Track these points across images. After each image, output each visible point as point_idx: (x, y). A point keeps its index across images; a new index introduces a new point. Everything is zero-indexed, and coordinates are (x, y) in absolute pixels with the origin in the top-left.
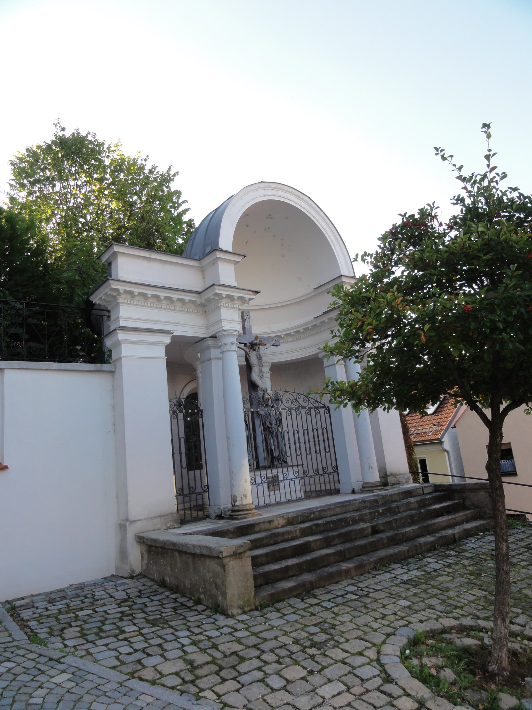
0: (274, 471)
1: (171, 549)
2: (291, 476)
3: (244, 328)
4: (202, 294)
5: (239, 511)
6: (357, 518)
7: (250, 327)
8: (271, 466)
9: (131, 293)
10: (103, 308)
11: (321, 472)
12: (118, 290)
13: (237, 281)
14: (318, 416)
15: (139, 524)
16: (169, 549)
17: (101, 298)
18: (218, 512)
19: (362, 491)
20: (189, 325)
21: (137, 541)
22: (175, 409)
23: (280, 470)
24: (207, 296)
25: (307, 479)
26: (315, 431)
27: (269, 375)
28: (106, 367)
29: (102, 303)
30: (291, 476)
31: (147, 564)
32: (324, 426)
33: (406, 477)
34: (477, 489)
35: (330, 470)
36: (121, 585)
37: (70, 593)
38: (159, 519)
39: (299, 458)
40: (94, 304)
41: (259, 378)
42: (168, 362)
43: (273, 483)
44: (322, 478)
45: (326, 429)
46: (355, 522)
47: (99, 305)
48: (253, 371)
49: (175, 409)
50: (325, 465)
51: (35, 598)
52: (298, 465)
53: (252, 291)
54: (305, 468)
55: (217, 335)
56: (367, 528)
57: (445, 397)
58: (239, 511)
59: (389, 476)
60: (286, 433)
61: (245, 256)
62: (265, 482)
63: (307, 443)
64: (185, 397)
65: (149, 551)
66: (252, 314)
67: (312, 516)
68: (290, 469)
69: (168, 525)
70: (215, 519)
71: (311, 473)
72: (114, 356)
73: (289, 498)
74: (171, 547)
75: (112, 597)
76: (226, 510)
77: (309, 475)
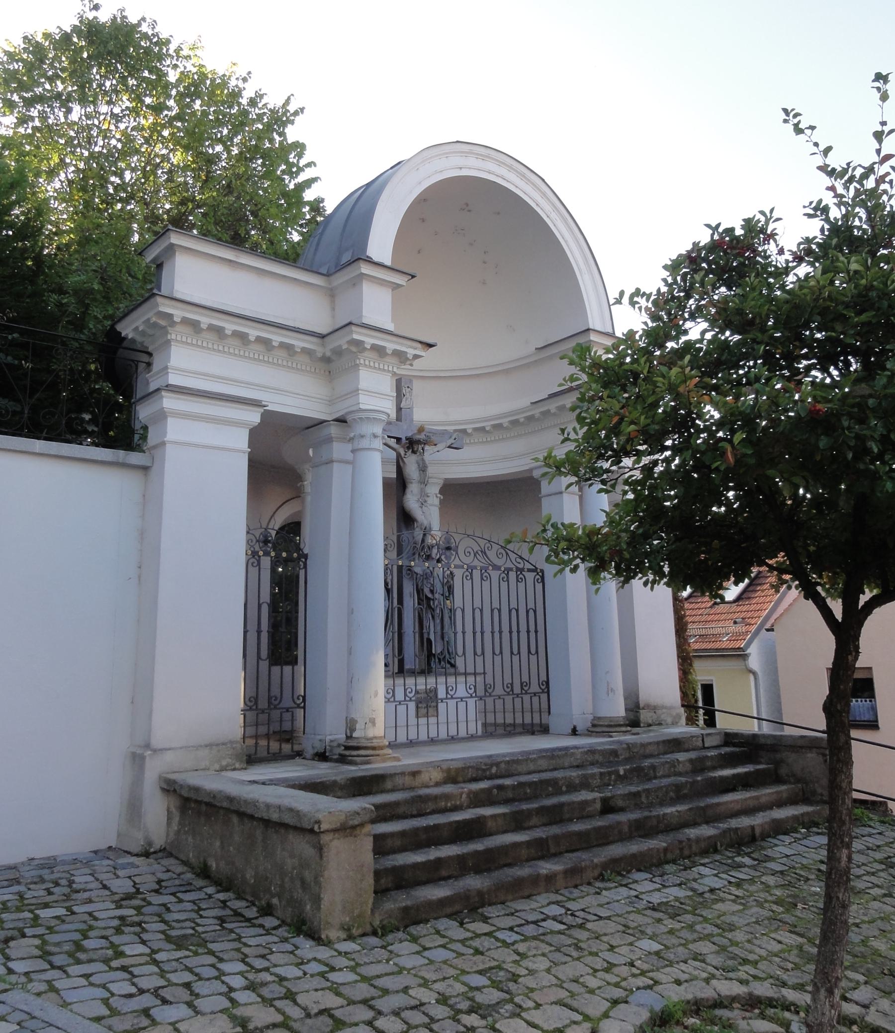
3: (399, 409)
4: (326, 339)
7: (411, 409)
8: (426, 671)
9: (195, 325)
10: (139, 347)
11: (517, 690)
13: (394, 319)
15: (169, 757)
19: (590, 733)
22: (257, 548)
25: (489, 701)
30: (461, 692)
31: (178, 832)
34: (801, 747)
39: (479, 660)
40: (124, 339)
43: (427, 703)
44: (518, 701)
45: (535, 611)
46: (572, 787)
47: (133, 341)
48: (408, 491)
49: (257, 548)
53: (421, 342)
55: (349, 418)
59: (643, 709)
60: (459, 613)
61: (413, 277)
62: (411, 700)
63: (497, 635)
64: (277, 528)
67: (494, 770)
68: (461, 679)
70: (313, 759)
73: (453, 732)
74: (225, 804)
75: (105, 887)
76: (335, 744)
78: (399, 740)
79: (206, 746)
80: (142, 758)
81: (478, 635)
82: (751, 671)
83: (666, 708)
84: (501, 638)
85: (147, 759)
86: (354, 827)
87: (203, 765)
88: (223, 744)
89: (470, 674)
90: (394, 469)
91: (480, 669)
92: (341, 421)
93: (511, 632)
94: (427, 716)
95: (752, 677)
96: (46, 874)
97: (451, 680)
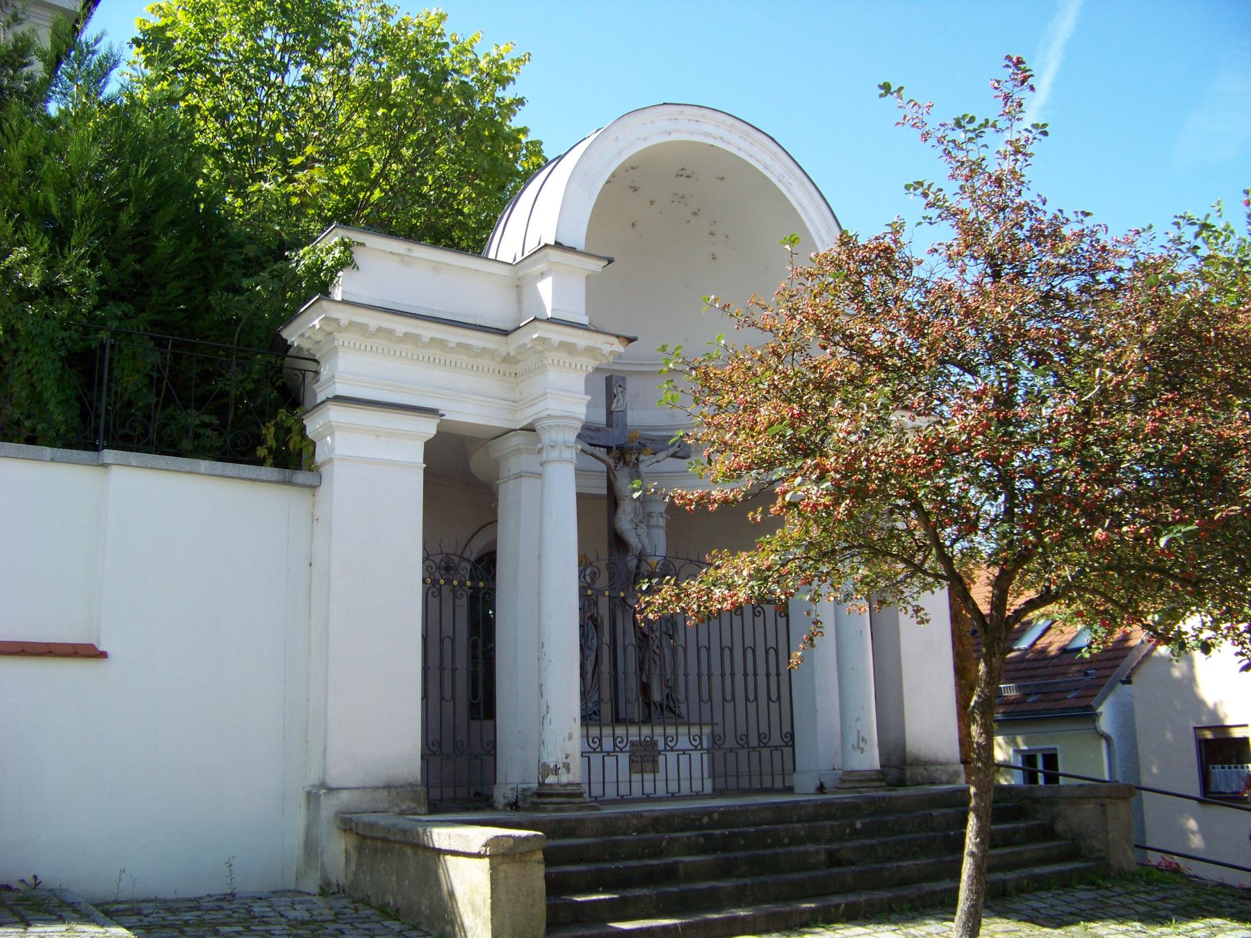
0: (646, 730)
1: (400, 843)
2: (683, 743)
3: (610, 413)
4: (510, 337)
5: (551, 795)
6: (802, 833)
7: (624, 412)
8: (647, 720)
9: (362, 328)
10: (306, 354)
11: (754, 742)
12: (337, 321)
13: (588, 312)
14: (759, 620)
15: (345, 796)
16: (395, 842)
17: (303, 335)
18: (511, 796)
19: (838, 789)
20: (473, 404)
21: (339, 828)
22: (437, 575)
23: (659, 730)
24: (522, 342)
25: (719, 754)
26: (749, 652)
27: (662, 522)
28: (302, 477)
29: (306, 345)
30: (683, 743)
31: (355, 873)
32: (771, 643)
33: (951, 769)
34: (1080, 798)
35: (776, 740)
36: (301, 902)
37: (204, 904)
38: (385, 793)
39: (706, 708)
40: (290, 346)
41: (633, 525)
42: (427, 473)
43: (644, 757)
44: (754, 755)
45: (776, 651)
46: (796, 840)
47: (299, 348)
48: (620, 510)
49: (437, 575)
50: (764, 729)
51: (143, 905)
52: (701, 725)
53: (618, 337)
54: (719, 730)
55: (538, 426)
56: (817, 852)
57: (278, 427)
58: (551, 795)
59: (911, 765)
60: (680, 651)
61: (610, 261)
62: (621, 750)
63: (728, 679)
64: (472, 559)
65: (360, 849)
66: (631, 384)
67: (705, 820)
68: (683, 730)
69: (404, 807)
70: (505, 810)
71: (730, 741)
72: (319, 457)
73: (673, 787)
74: (399, 837)
75: (282, 916)
76: (529, 793)
77: (726, 745)
78: (607, 796)
79: (384, 787)
80: (318, 796)
81: (705, 678)
82: (1104, 736)
83: (940, 764)
84: (733, 682)
85: (323, 799)
86: (524, 854)
87: (381, 807)
88: (402, 787)
89: (694, 724)
90: (604, 483)
91: (706, 717)
92: (530, 429)
93: (745, 675)
94: (642, 772)
95: (1104, 744)
96: (224, 904)
97: (671, 730)
